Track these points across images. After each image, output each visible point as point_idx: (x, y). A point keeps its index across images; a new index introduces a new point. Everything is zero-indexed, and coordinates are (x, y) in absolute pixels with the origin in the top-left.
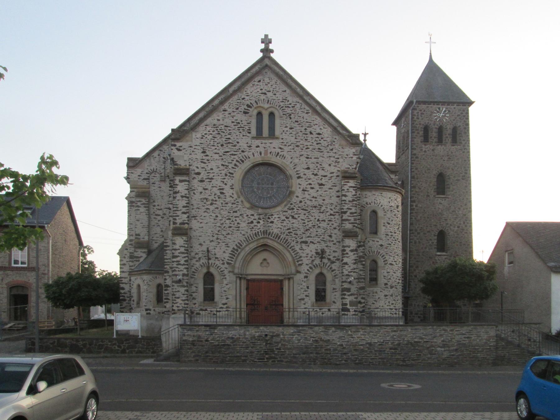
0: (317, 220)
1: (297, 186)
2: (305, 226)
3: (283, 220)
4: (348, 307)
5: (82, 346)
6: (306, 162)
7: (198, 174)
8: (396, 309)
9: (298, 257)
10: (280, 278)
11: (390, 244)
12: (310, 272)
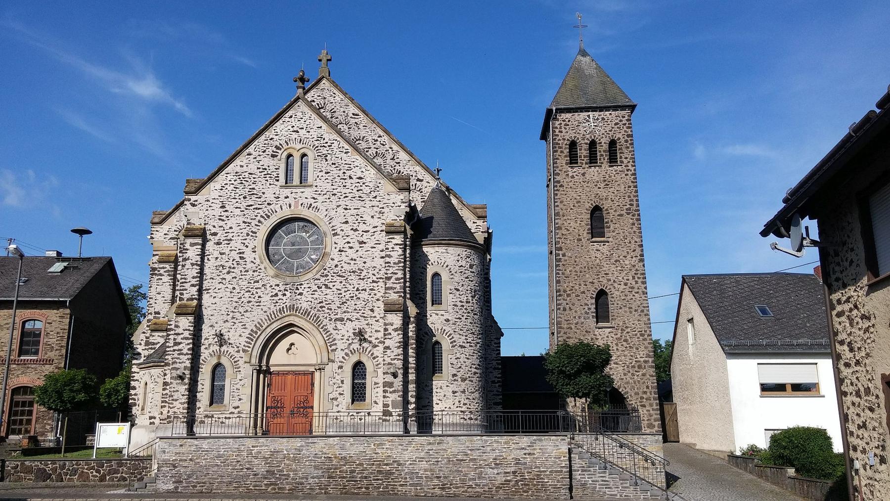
0: (356, 289)
1: (331, 245)
2: (342, 297)
3: (314, 291)
4: (390, 409)
5: (51, 472)
6: (344, 214)
7: (215, 234)
8: (471, 412)
9: (331, 340)
10: (312, 369)
11: (460, 319)
12: (345, 360)
